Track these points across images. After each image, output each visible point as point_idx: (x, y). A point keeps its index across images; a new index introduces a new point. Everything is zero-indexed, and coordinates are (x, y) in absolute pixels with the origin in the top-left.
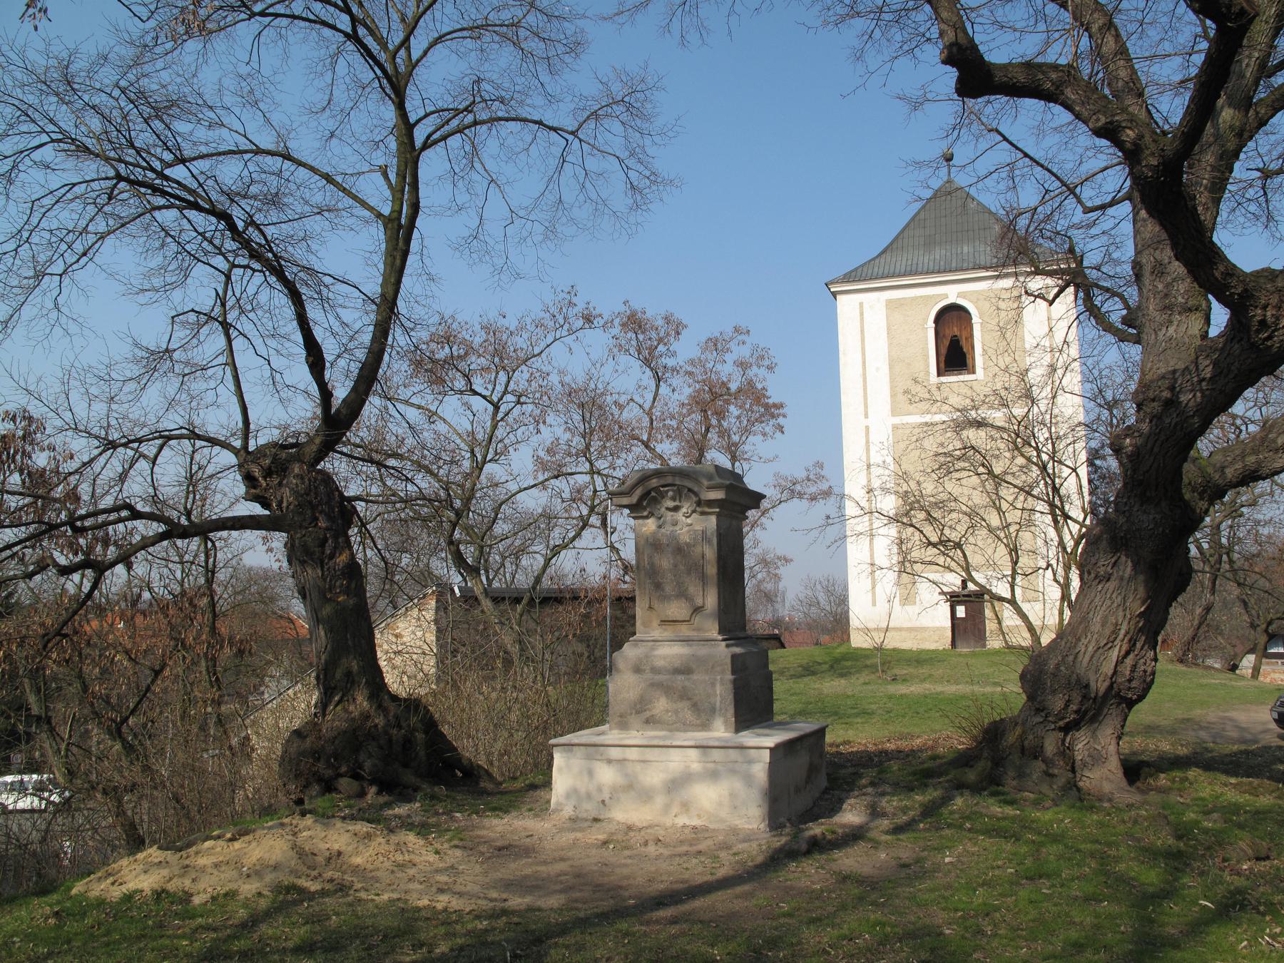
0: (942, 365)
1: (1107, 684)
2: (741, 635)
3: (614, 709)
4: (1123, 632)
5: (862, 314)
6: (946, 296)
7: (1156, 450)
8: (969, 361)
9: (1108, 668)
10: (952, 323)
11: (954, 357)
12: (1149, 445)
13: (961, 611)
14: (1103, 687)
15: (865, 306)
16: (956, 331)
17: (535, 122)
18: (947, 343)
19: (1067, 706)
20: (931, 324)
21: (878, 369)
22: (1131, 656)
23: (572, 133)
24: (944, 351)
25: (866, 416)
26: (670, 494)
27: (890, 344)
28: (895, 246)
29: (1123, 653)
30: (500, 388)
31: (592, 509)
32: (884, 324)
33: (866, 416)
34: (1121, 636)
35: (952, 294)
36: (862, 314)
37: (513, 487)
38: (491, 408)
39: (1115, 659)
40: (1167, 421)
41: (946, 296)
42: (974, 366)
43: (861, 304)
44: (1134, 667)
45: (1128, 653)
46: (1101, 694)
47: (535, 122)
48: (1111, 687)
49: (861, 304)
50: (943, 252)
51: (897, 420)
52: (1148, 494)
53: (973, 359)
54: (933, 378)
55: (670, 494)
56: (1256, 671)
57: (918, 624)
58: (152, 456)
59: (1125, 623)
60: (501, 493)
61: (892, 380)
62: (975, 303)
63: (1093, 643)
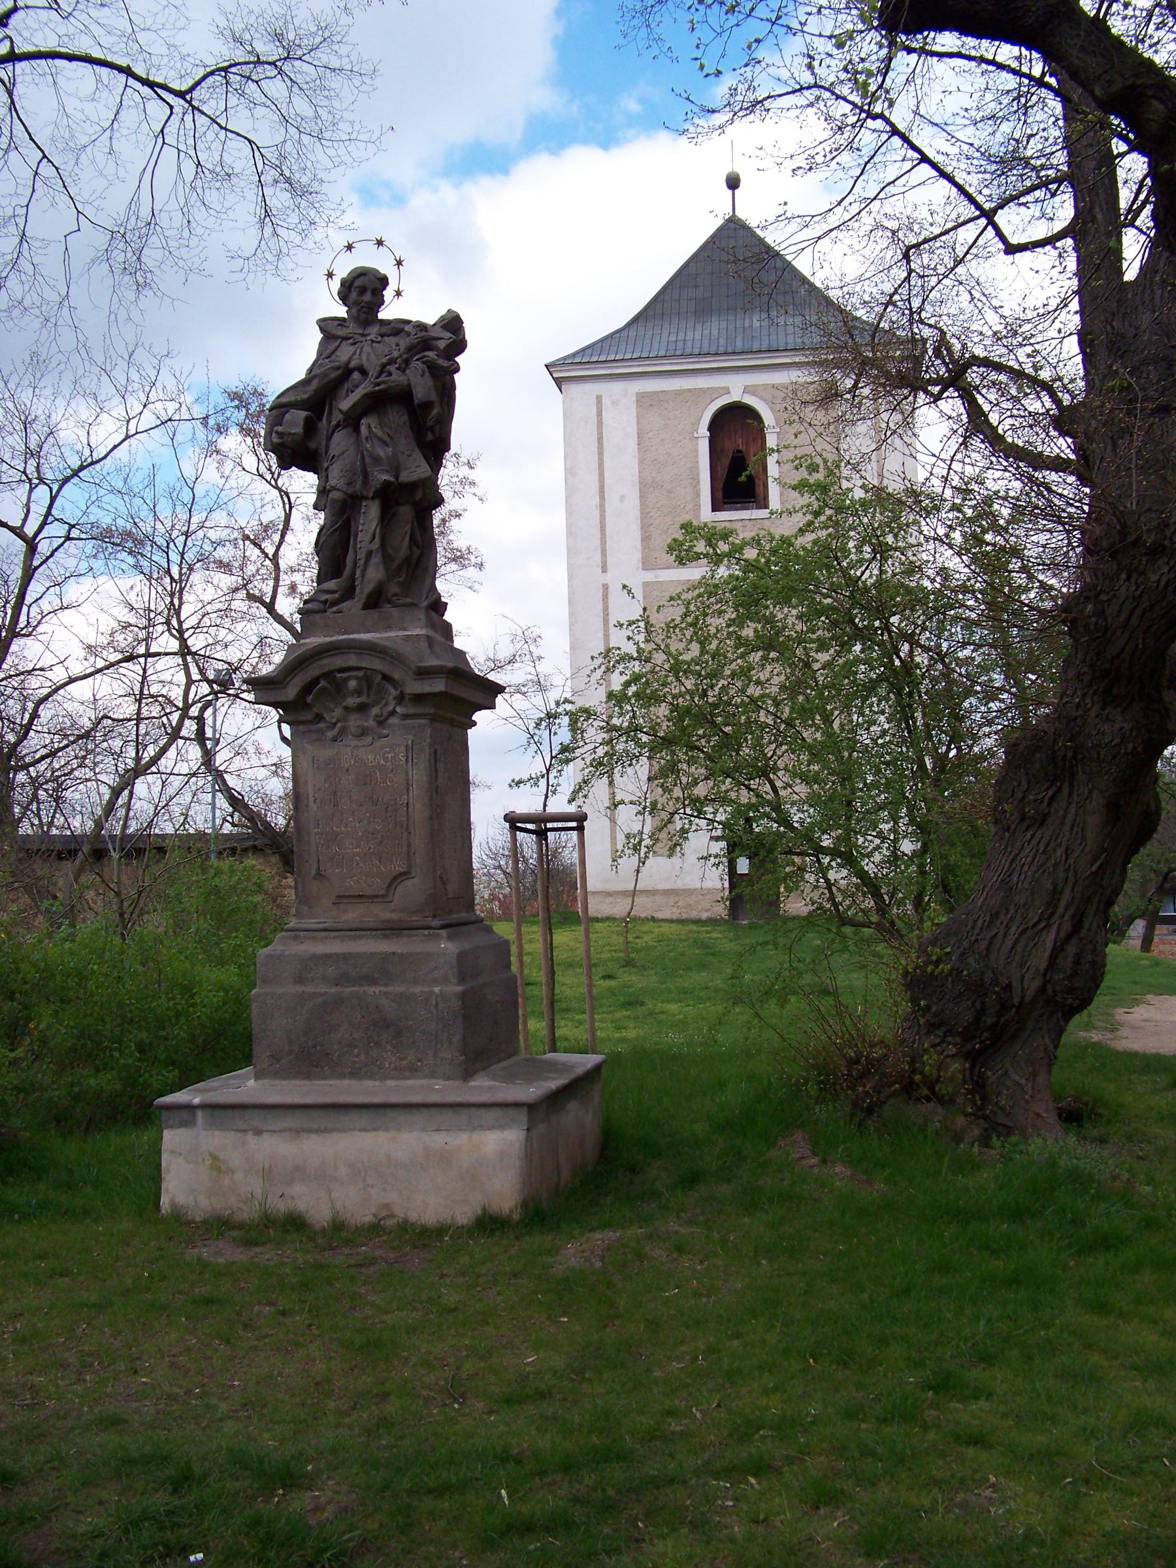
0: (720, 495)
1: (1037, 983)
2: (464, 916)
3: (261, 1051)
4: (1063, 904)
5: (599, 414)
6: (727, 391)
7: (1134, 621)
8: (759, 489)
9: (1040, 959)
10: (735, 430)
11: (737, 484)
12: (1124, 616)
13: (743, 866)
14: (1032, 987)
15: (605, 401)
16: (740, 443)
17: (120, 69)
18: (726, 461)
19: (977, 1019)
20: (703, 431)
21: (622, 498)
22: (1075, 941)
23: (180, 94)
24: (723, 473)
25: (604, 569)
26: (352, 684)
27: (641, 462)
28: (651, 313)
29: (1063, 935)
30: (38, 510)
31: (185, 715)
32: (633, 429)
33: (604, 569)
34: (1060, 911)
35: (735, 388)
36: (599, 414)
37: (59, 675)
38: (20, 545)
39: (1049, 945)
40: (1154, 578)
41: (727, 391)
42: (766, 498)
43: (599, 399)
44: (1078, 957)
45: (1069, 937)
46: (1028, 999)
47: (120, 69)
48: (1042, 989)
49: (599, 399)
50: (723, 325)
51: (650, 576)
52: (1115, 692)
53: (766, 486)
54: (706, 514)
55: (352, 684)
56: (1147, 942)
57: (679, 885)
58: (152, 650)
59: (1068, 890)
60: (37, 685)
61: (644, 514)
62: (771, 403)
63: (1018, 921)
